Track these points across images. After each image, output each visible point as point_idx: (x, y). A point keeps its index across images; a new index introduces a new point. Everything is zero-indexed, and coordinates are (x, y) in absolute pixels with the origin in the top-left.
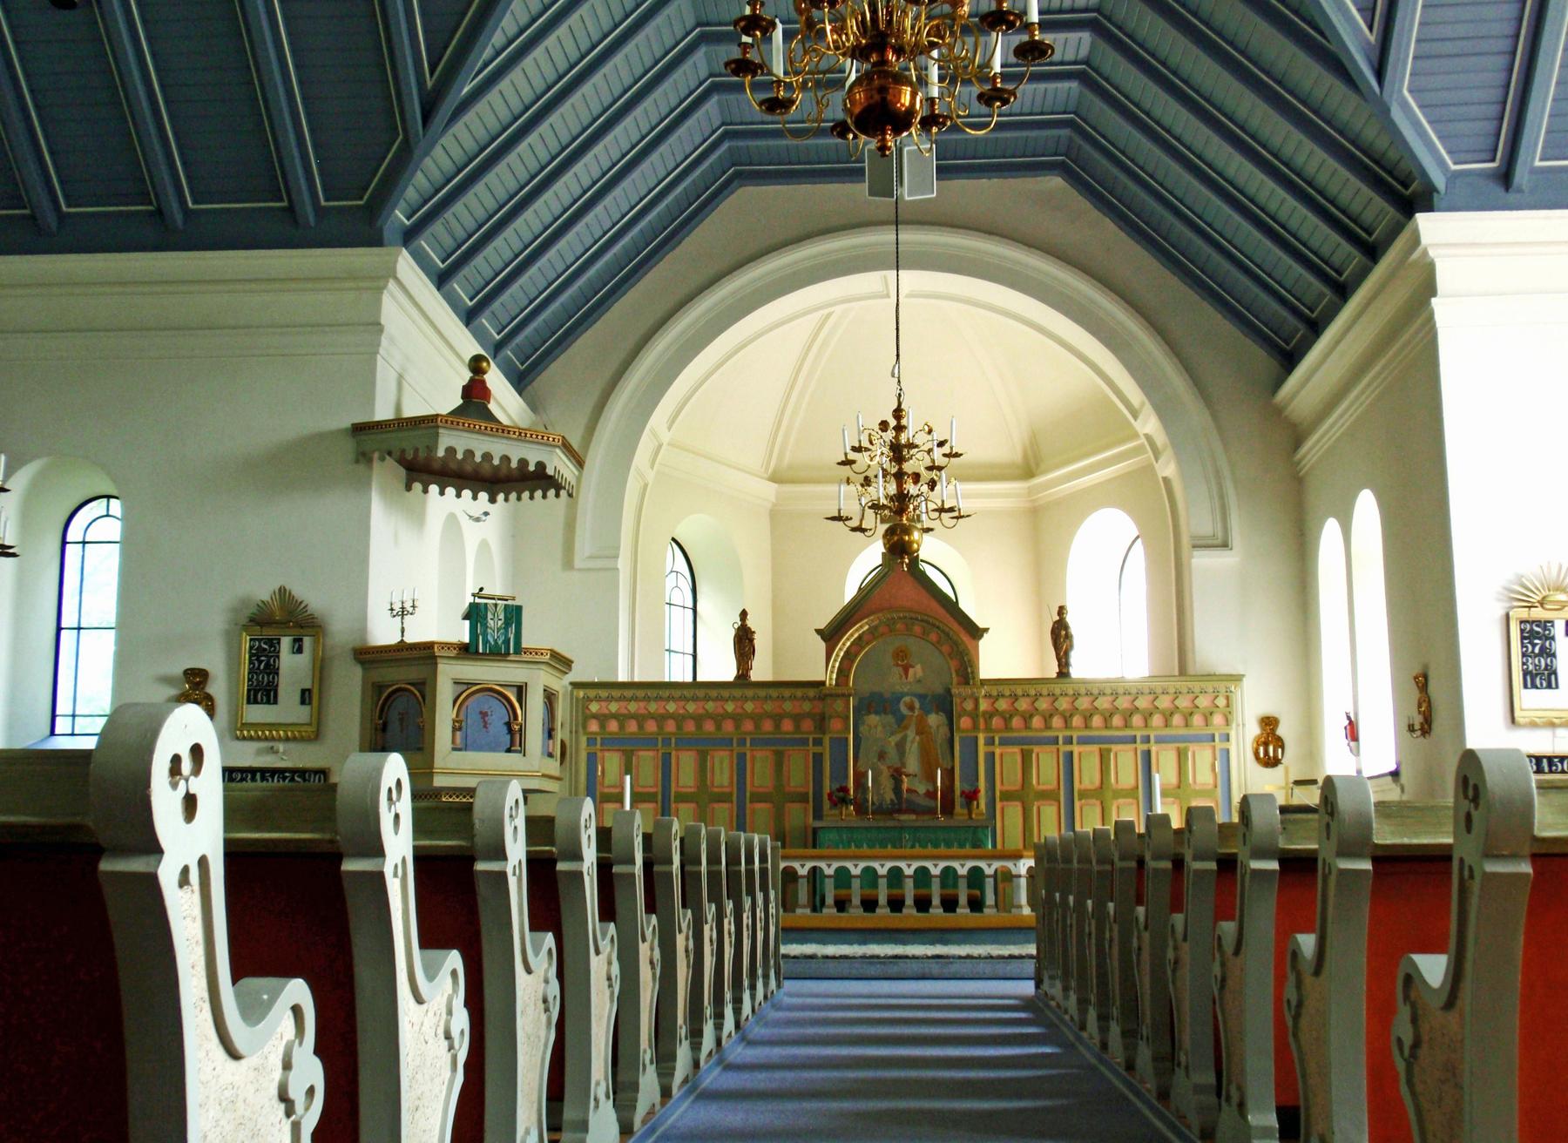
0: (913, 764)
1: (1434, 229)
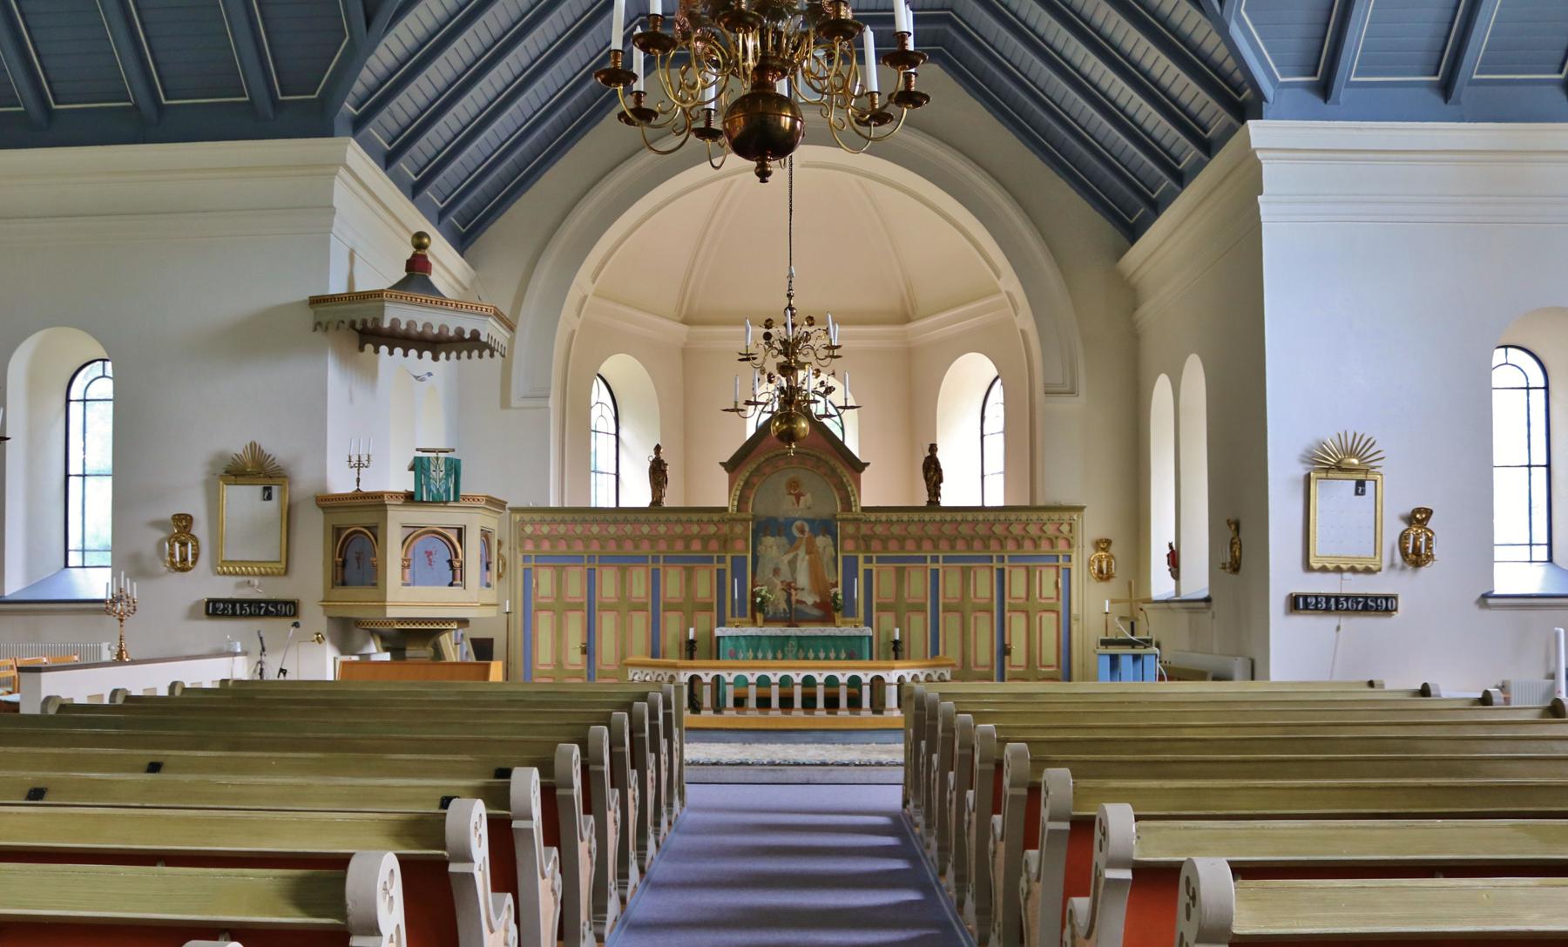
0: (803, 579)
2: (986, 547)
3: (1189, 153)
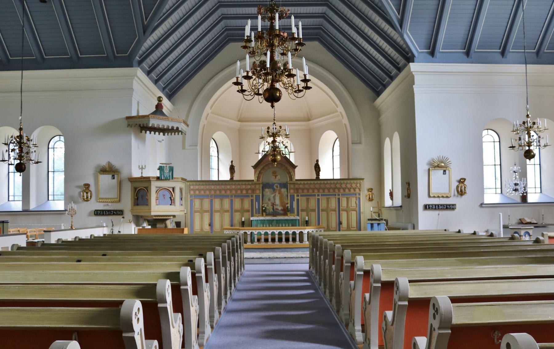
0: (278, 202)
1: (413, 67)
2: (334, 191)
3: (394, 71)
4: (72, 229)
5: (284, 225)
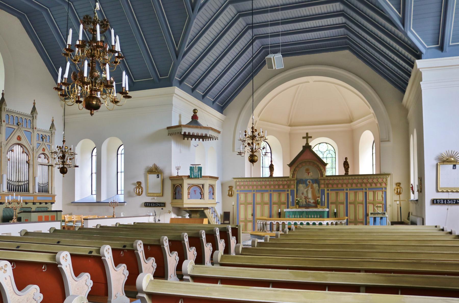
0: (310, 195)
2: (361, 186)
4: (113, 217)
5: (316, 216)
